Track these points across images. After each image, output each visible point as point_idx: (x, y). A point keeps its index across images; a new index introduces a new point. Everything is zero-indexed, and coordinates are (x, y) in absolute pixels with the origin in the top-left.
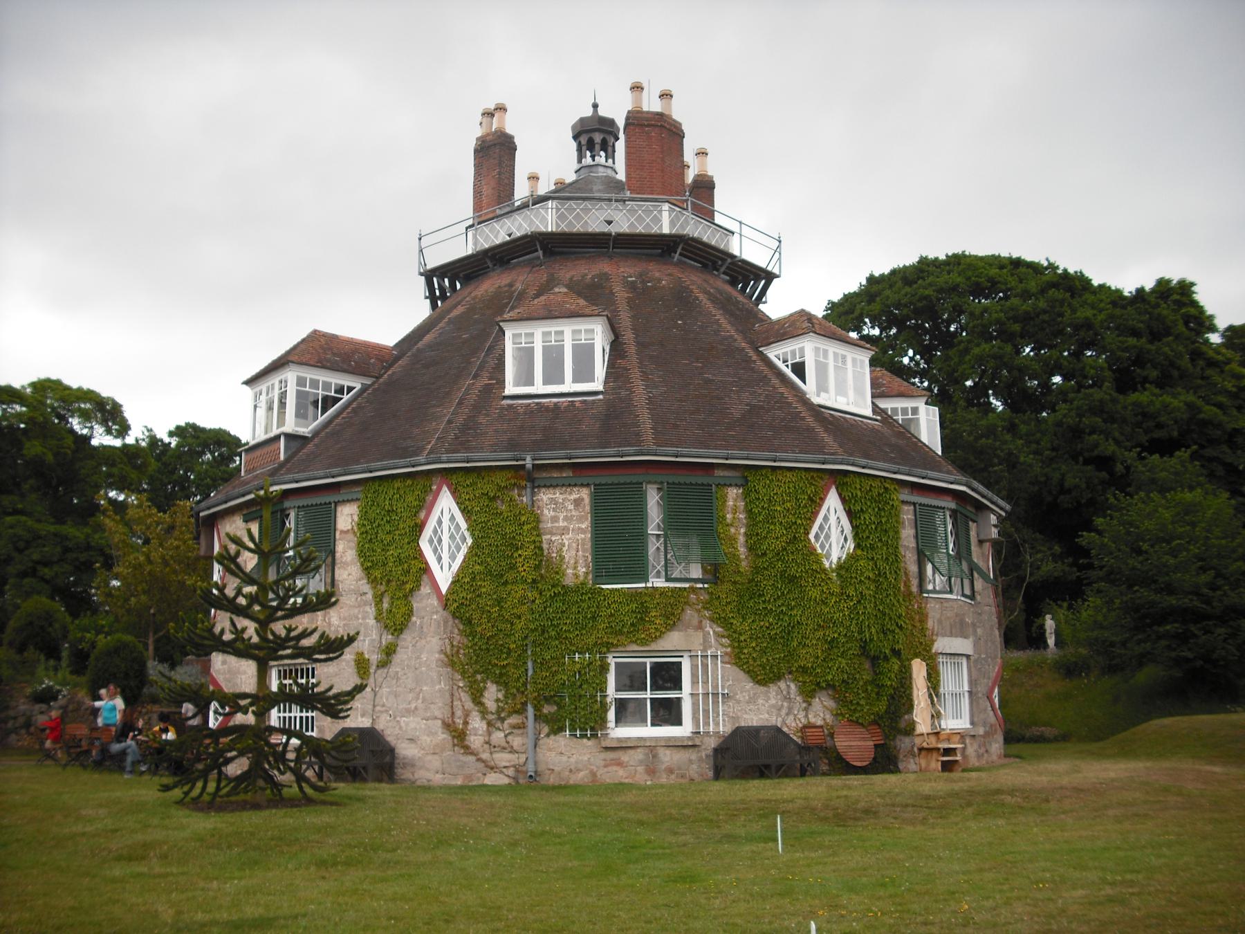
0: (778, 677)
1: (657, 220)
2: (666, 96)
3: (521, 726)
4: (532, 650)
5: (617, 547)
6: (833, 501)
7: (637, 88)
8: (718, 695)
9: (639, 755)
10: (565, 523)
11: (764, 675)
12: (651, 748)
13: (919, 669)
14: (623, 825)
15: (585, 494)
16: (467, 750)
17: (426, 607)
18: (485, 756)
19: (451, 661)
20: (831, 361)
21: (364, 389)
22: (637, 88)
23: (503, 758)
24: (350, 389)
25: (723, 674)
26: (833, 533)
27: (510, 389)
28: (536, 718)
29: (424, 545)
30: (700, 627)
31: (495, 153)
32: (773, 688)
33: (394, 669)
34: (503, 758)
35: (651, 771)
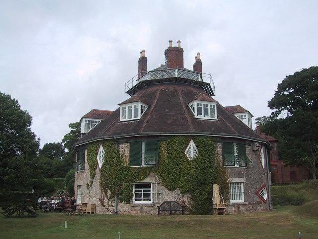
0: (175, 189)
1: (174, 74)
2: (179, 42)
3: (114, 200)
4: (120, 184)
5: (135, 157)
6: (192, 144)
7: (171, 42)
8: (160, 194)
9: (138, 208)
10: (124, 149)
11: (171, 189)
12: (142, 206)
13: (216, 188)
14: (131, 224)
15: (129, 145)
16: (104, 206)
17: (98, 172)
18: (107, 207)
19: (101, 185)
20: (209, 107)
21: (102, 122)
22: (171, 42)
23: (111, 208)
24: (99, 122)
25: (160, 188)
26: (192, 151)
27: (121, 120)
28: (117, 198)
29: (98, 158)
30: (154, 176)
31: (143, 61)
32: (174, 192)
33: (93, 186)
34: (111, 208)
35: (141, 212)
